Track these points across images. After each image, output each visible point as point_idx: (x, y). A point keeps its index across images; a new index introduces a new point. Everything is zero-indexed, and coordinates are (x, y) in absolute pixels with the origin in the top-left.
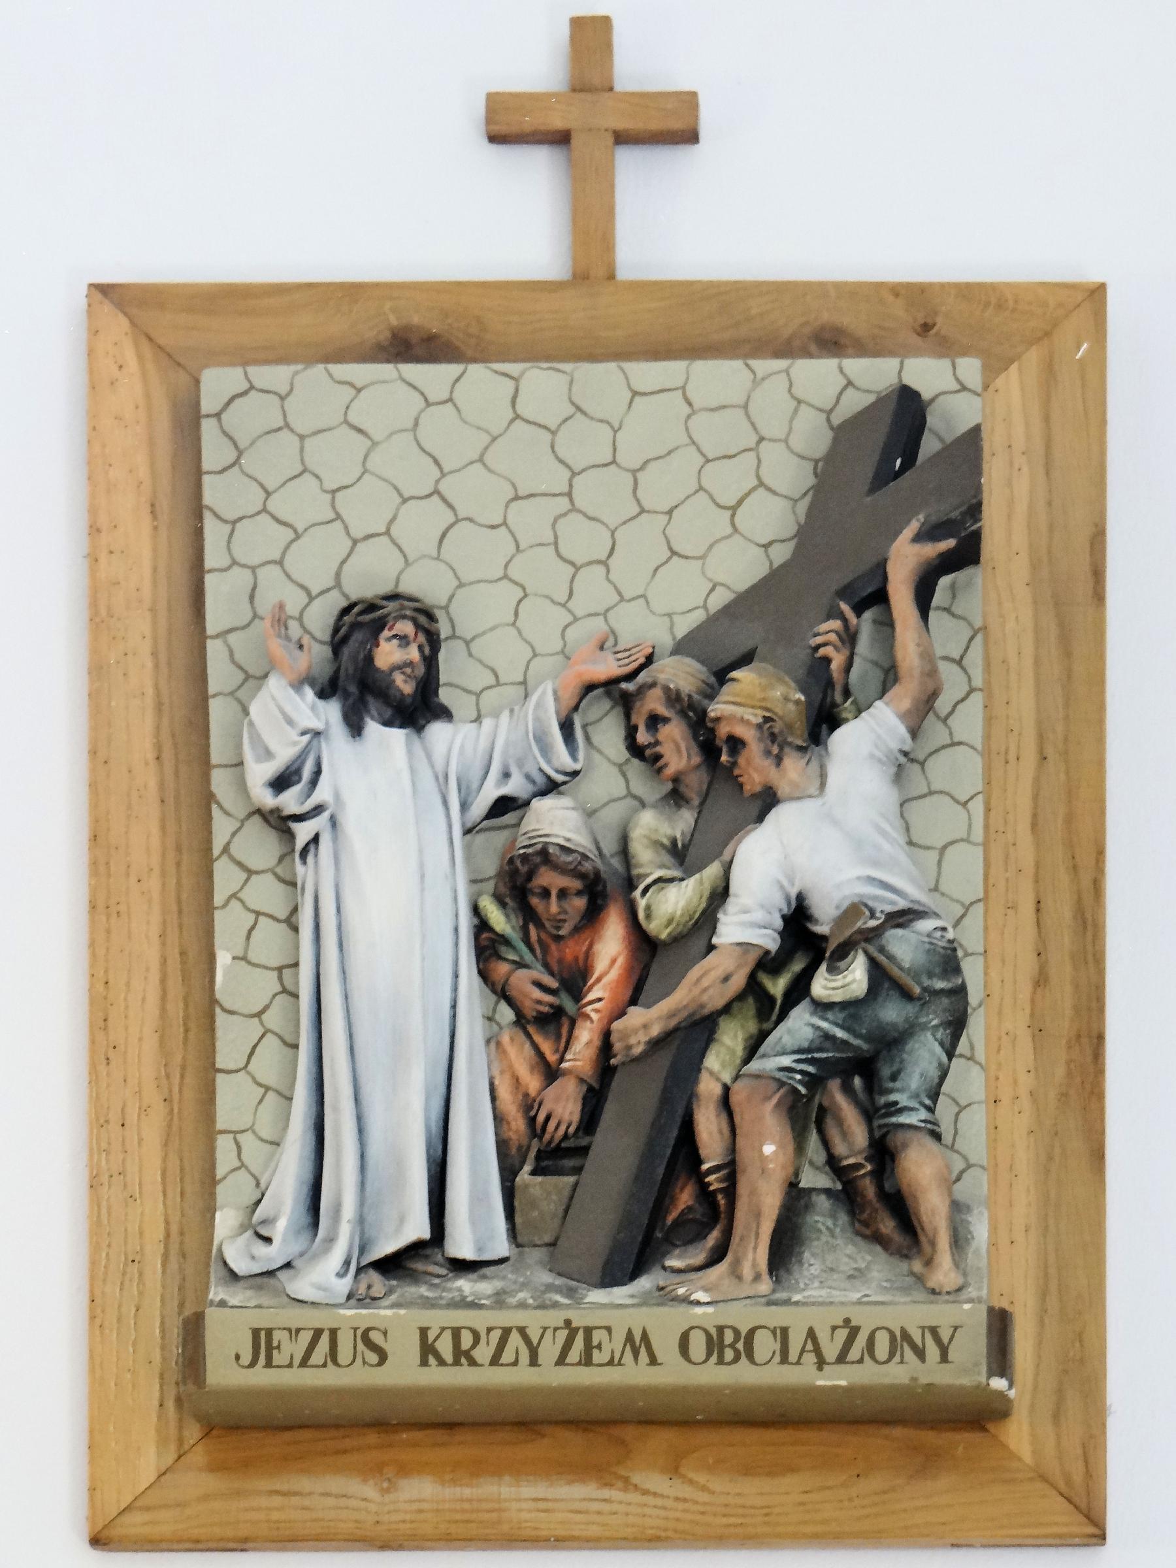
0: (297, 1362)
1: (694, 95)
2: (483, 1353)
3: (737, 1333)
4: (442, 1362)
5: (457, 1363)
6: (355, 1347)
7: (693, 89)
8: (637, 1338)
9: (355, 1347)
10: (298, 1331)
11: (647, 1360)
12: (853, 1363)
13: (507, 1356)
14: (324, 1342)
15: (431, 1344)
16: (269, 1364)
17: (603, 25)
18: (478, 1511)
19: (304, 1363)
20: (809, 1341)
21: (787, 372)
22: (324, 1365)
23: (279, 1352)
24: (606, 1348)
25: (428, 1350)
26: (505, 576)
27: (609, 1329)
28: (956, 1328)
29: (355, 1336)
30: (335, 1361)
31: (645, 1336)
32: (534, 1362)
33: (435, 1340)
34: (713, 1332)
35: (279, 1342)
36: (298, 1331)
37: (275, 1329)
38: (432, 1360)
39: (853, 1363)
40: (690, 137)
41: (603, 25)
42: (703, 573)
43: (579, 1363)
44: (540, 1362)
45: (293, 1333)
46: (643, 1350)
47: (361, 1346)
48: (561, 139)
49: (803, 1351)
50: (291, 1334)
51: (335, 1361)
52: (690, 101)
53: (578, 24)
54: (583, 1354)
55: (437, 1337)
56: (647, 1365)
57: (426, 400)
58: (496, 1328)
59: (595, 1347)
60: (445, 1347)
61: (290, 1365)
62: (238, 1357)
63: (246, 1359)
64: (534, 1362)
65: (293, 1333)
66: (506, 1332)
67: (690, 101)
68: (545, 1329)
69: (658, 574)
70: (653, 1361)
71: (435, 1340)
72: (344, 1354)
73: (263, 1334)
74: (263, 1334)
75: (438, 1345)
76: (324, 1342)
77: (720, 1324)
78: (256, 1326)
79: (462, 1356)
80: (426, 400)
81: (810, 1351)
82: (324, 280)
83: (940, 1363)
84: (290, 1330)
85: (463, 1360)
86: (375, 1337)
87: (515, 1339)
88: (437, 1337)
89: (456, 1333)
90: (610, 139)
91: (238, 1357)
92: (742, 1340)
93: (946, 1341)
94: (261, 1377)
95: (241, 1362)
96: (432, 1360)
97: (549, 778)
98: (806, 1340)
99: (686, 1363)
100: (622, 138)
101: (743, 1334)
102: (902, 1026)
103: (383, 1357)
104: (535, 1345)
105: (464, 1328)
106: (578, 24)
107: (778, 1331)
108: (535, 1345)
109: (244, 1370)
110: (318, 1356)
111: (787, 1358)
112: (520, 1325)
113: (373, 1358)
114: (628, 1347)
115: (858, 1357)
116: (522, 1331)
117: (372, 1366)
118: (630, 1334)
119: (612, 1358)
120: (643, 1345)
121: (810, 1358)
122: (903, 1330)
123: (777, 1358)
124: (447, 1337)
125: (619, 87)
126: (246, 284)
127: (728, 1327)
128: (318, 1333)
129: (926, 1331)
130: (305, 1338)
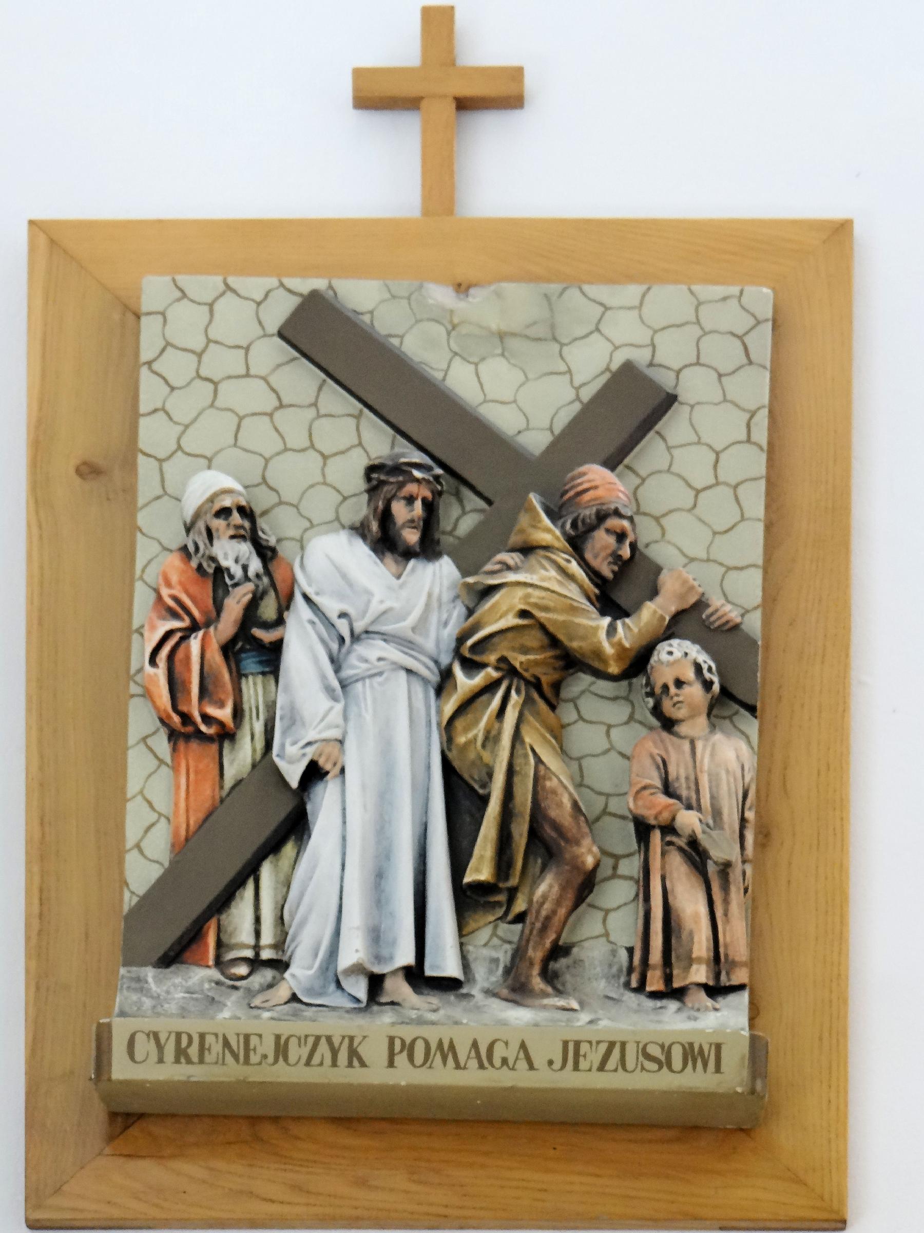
1: (452, 8)
5: (177, 1061)
6: (638, 1058)
7: (513, 62)
9: (638, 1058)
12: (254, 1065)
13: (316, 1059)
14: (616, 1053)
16: (576, 1067)
17: (447, 13)
18: (307, 1205)
19: (601, 1068)
22: (616, 1070)
24: (260, 1051)
25: (181, 1054)
26: (698, 492)
27: (260, 1036)
28: (365, 1037)
29: (638, 1046)
30: (624, 1068)
31: (452, 1047)
32: (334, 1064)
34: (687, 1046)
35: (210, 1045)
36: (598, 1042)
38: (356, 1062)
39: (254, 1065)
41: (447, 13)
42: (206, 331)
44: (395, 1065)
45: (594, 1044)
47: (641, 1058)
51: (624, 1068)
52: (517, 74)
53: (428, 14)
55: (360, 1044)
57: (724, 395)
63: (558, 1064)
64: (334, 1064)
65: (594, 1044)
66: (318, 1039)
67: (517, 74)
70: (531, 1067)
72: (630, 1063)
75: (360, 1050)
78: (565, 1038)
80: (724, 395)
85: (183, 1060)
87: (323, 1047)
88: (360, 1044)
89: (178, 1035)
91: (551, 1063)
93: (336, 1045)
94: (569, 1080)
96: (356, 1062)
98: (519, 1052)
104: (337, 1048)
105: (183, 1032)
106: (428, 14)
108: (337, 1048)
112: (328, 1033)
115: (613, 1067)
116: (329, 1039)
120: (446, 1052)
121: (473, 1063)
122: (701, 1047)
124: (173, 1038)
126: (307, 219)
128: (612, 1045)
130: (603, 1048)
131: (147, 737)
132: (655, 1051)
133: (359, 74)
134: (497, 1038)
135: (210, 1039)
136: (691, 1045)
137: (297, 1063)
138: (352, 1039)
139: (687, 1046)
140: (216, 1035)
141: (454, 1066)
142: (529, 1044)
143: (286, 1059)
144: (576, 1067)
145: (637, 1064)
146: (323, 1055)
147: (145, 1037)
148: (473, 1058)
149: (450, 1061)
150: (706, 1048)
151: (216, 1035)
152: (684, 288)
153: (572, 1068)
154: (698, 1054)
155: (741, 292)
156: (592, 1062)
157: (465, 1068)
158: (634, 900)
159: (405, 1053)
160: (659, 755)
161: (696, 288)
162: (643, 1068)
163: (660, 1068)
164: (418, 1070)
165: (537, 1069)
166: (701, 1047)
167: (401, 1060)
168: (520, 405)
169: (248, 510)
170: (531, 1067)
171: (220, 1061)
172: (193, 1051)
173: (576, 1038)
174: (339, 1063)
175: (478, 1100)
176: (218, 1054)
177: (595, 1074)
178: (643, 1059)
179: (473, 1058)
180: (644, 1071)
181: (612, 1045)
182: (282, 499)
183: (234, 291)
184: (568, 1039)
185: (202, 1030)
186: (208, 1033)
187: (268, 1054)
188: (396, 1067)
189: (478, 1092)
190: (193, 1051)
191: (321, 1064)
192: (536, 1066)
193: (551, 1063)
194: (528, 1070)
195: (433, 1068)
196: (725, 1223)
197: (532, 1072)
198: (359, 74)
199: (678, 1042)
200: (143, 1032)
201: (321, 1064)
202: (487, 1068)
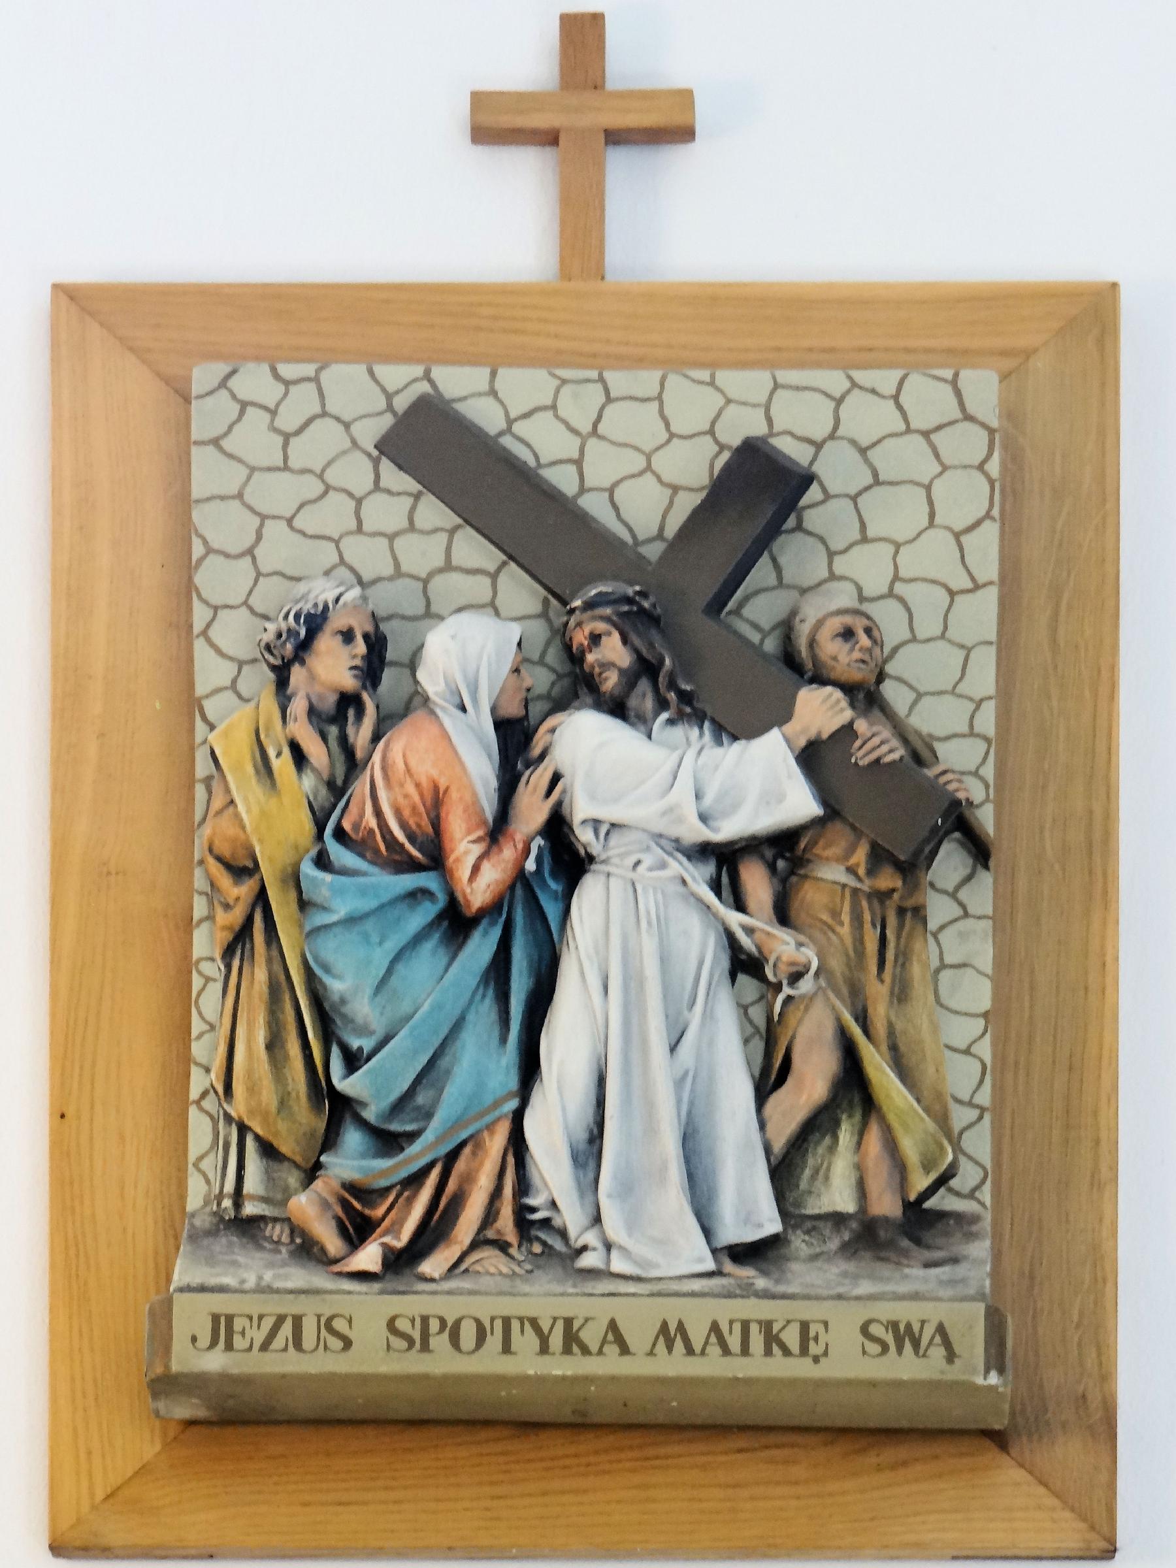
0: (257, 1345)
3: (443, 1322)
4: (787, 1352)
5: (567, 1350)
8: (672, 1328)
10: (261, 1317)
11: (780, 1353)
14: (287, 1329)
15: (776, 1335)
16: (229, 1347)
19: (265, 1347)
20: (713, 1334)
21: (316, 380)
28: (587, 1320)
29: (319, 1321)
31: (681, 1327)
32: (544, 1349)
33: (579, 1329)
40: (685, 134)
46: (679, 1340)
48: (551, 138)
49: (930, 1343)
52: (685, 98)
55: (784, 1328)
56: (684, 1355)
60: (791, 1337)
62: (194, 1339)
63: (205, 1339)
67: (685, 98)
68: (555, 1319)
69: (296, 574)
70: (625, 1350)
71: (579, 1329)
73: (223, 1320)
74: (223, 1320)
75: (582, 1335)
76: (287, 1329)
77: (744, 1318)
81: (939, 1345)
83: (538, 1354)
84: (251, 1318)
86: (340, 1325)
90: (602, 138)
91: (194, 1339)
92: (448, 1329)
93: (546, 1330)
94: (560, 1366)
95: (198, 1344)
100: (615, 137)
101: (449, 1325)
102: (359, 1019)
103: (348, 1343)
104: (937, 1334)
109: (474, 1357)
110: (278, 1342)
111: (548, 1347)
113: (336, 1344)
117: (874, 1357)
118: (664, 1326)
120: (672, 1336)
128: (281, 1319)
129: (526, 1323)
133: (479, 100)
134: (398, 1313)
138: (568, 1322)
141: (684, 1351)
142: (946, 1325)
144: (229, 1347)
146: (827, 1345)
149: (679, 1344)
152: (362, 368)
154: (905, 1339)
155: (956, 375)
156: (252, 1339)
158: (211, 1148)
159: (446, 1335)
160: (882, 981)
161: (380, 370)
162: (326, 1347)
164: (466, 1357)
167: (440, 1342)
169: (289, 691)
170: (625, 1350)
173: (230, 1311)
174: (752, 1349)
175: (596, 1388)
176: (287, 1339)
185: (425, 1313)
186: (814, 1321)
188: (515, 1354)
189: (772, 1383)
194: (684, 1355)
195: (655, 1355)
197: (627, 1358)
198: (479, 100)
202: (576, 1355)
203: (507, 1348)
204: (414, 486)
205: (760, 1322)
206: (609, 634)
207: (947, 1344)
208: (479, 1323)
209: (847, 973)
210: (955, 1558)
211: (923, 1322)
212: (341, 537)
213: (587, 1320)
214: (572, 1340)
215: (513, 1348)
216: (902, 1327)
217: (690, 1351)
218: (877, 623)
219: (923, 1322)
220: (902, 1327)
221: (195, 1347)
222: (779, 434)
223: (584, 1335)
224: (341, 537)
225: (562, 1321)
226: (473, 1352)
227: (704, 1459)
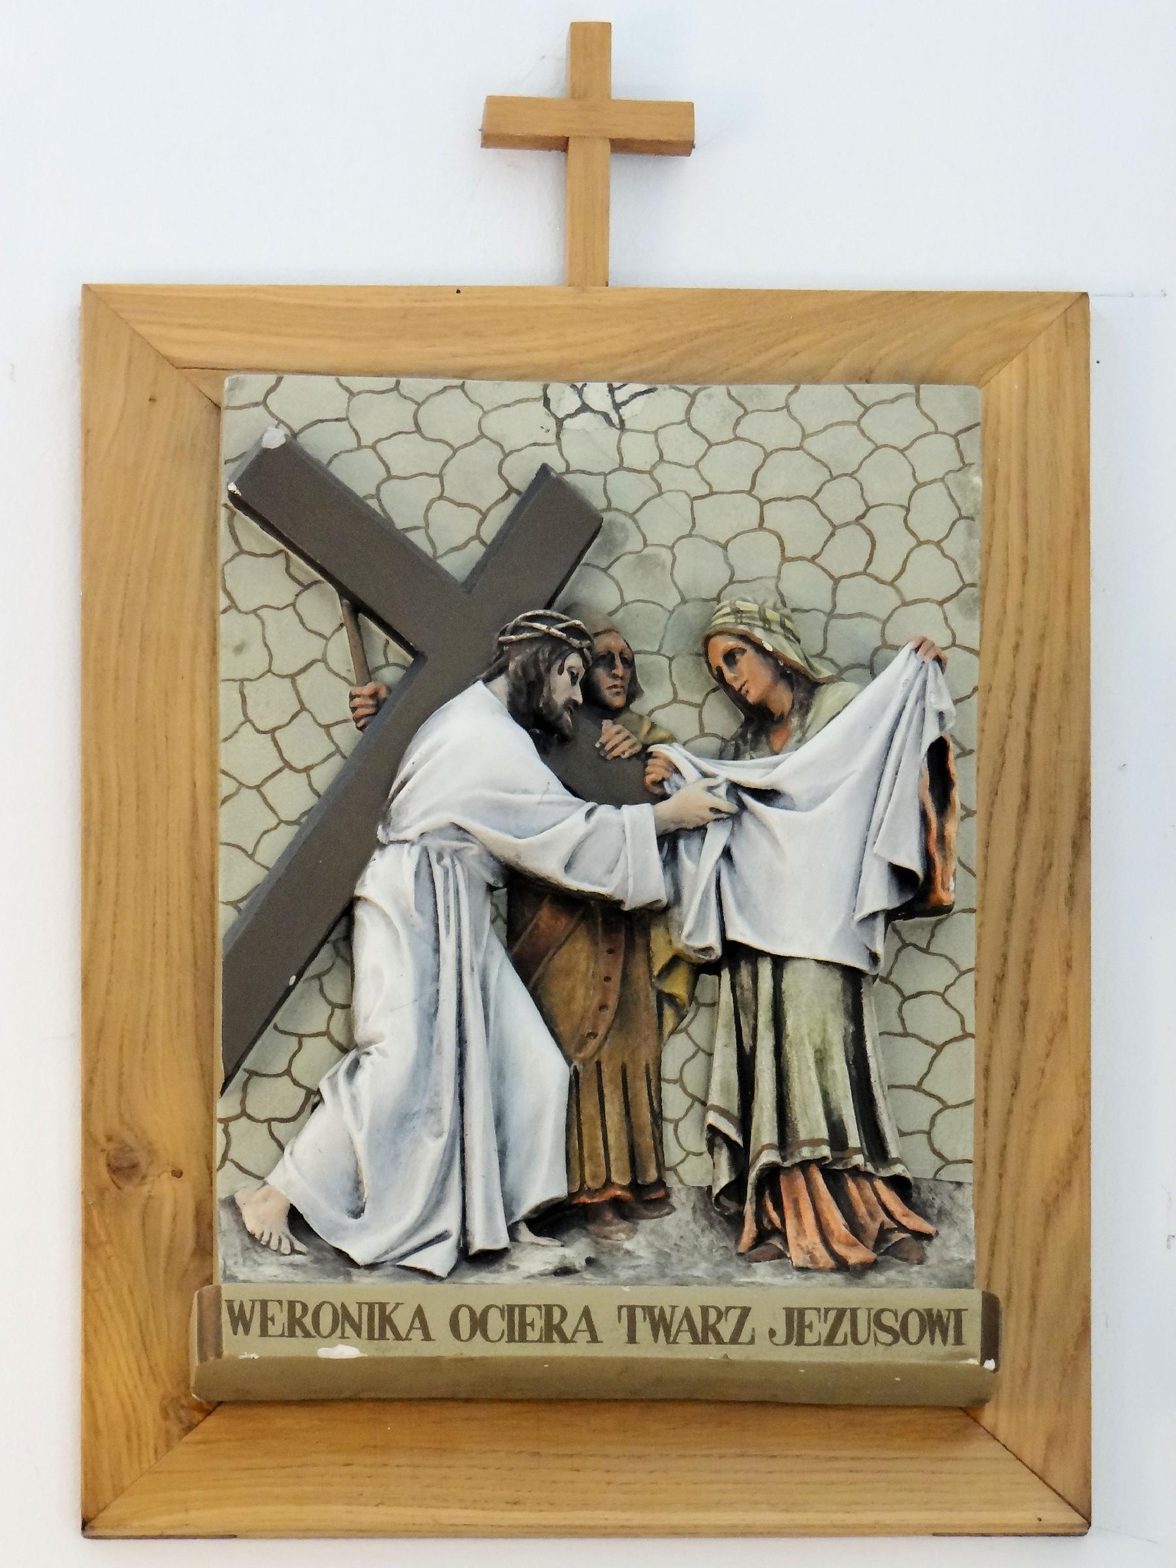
0: (823, 1339)
1: (691, 105)
2: (726, 1329)
3: (305, 1308)
6: (869, 1328)
9: (869, 1328)
14: (846, 1327)
19: (830, 1340)
20: (417, 1320)
23: (273, 1324)
25: (294, 1325)
28: (398, 1304)
29: (869, 1315)
30: (855, 1340)
33: (392, 1312)
34: (925, 1314)
37: (806, 1309)
40: (685, 147)
43: (540, 1341)
48: (562, 145)
49: (679, 1331)
50: (541, 1310)
51: (855, 1340)
54: (286, 1325)
55: (395, 1309)
58: (735, 1308)
59: (529, 1325)
61: (818, 1343)
63: (781, 1335)
65: (823, 1312)
67: (687, 110)
71: (392, 1312)
73: (517, 1311)
79: (552, 1331)
82: (817, 288)
84: (818, 1310)
85: (555, 1337)
89: (292, 1305)
91: (772, 1333)
95: (775, 1340)
97: (649, 774)
99: (450, 1334)
100: (621, 146)
104: (417, 1319)
105: (554, 1305)
107: (543, 1308)
108: (417, 1319)
109: (894, 1346)
114: (357, 1319)
119: (820, 1341)
123: (505, 1338)
125: (615, 95)
127: (298, 1302)
128: (841, 1313)
129: (952, 1313)
131: (921, 949)
132: (888, 1319)
133: (496, 105)
135: (273, 1309)
136: (929, 1311)
137: (500, 1340)
139: (925, 1314)
140: (280, 1302)
141: (626, 1338)
143: (485, 1335)
144: (264, 1332)
145: (869, 1335)
147: (498, 1313)
148: (417, 1329)
150: (945, 1314)
151: (280, 1302)
153: (258, 1332)
157: (572, 1341)
162: (876, 1340)
163: (896, 1340)
165: (433, 1340)
166: (662, 1310)
168: (432, 534)
170: (427, 1337)
171: (286, 1334)
172: (308, 1321)
177: (822, 1349)
178: (875, 1328)
179: (417, 1329)
180: (410, 1337)
181: (841, 1313)
182: (272, 668)
183: (692, 403)
184: (794, 1306)
187: (777, 1332)
190: (308, 1321)
191: (752, 1341)
192: (433, 1334)
193: (772, 1333)
196: (938, 1531)
198: (496, 105)
199: (329, 1303)
200: (497, 1307)
201: (752, 1341)
203: (632, 1339)
204: (568, 478)
205: (643, 1308)
206: (743, 651)
207: (591, 1329)
208: (335, 1310)
209: (665, 974)
210: (935, 1535)
211: (673, 1308)
212: (378, 489)
213: (398, 1304)
214: (552, 1331)
215: (964, 1339)
216: (657, 1312)
217: (398, 1337)
218: (959, 698)
219: (673, 1308)
220: (657, 1312)
221: (462, 1341)
222: (574, 472)
223: (395, 1318)
224: (378, 489)
225: (259, 1303)
226: (468, 1340)
227: (708, 1452)
